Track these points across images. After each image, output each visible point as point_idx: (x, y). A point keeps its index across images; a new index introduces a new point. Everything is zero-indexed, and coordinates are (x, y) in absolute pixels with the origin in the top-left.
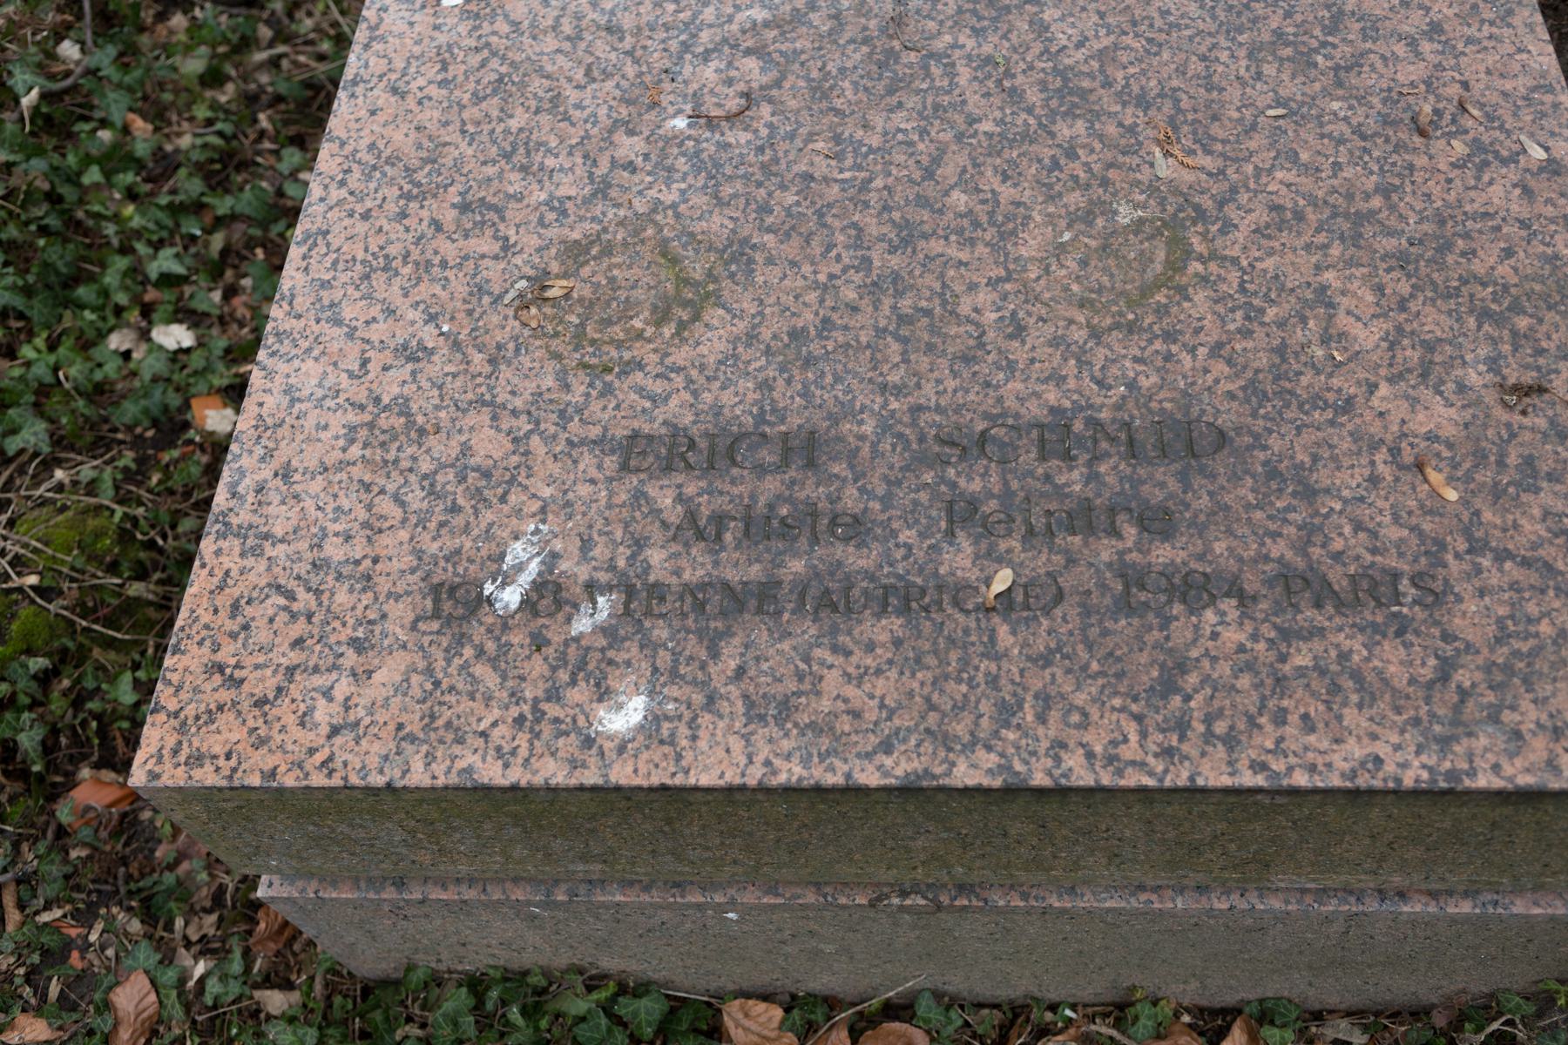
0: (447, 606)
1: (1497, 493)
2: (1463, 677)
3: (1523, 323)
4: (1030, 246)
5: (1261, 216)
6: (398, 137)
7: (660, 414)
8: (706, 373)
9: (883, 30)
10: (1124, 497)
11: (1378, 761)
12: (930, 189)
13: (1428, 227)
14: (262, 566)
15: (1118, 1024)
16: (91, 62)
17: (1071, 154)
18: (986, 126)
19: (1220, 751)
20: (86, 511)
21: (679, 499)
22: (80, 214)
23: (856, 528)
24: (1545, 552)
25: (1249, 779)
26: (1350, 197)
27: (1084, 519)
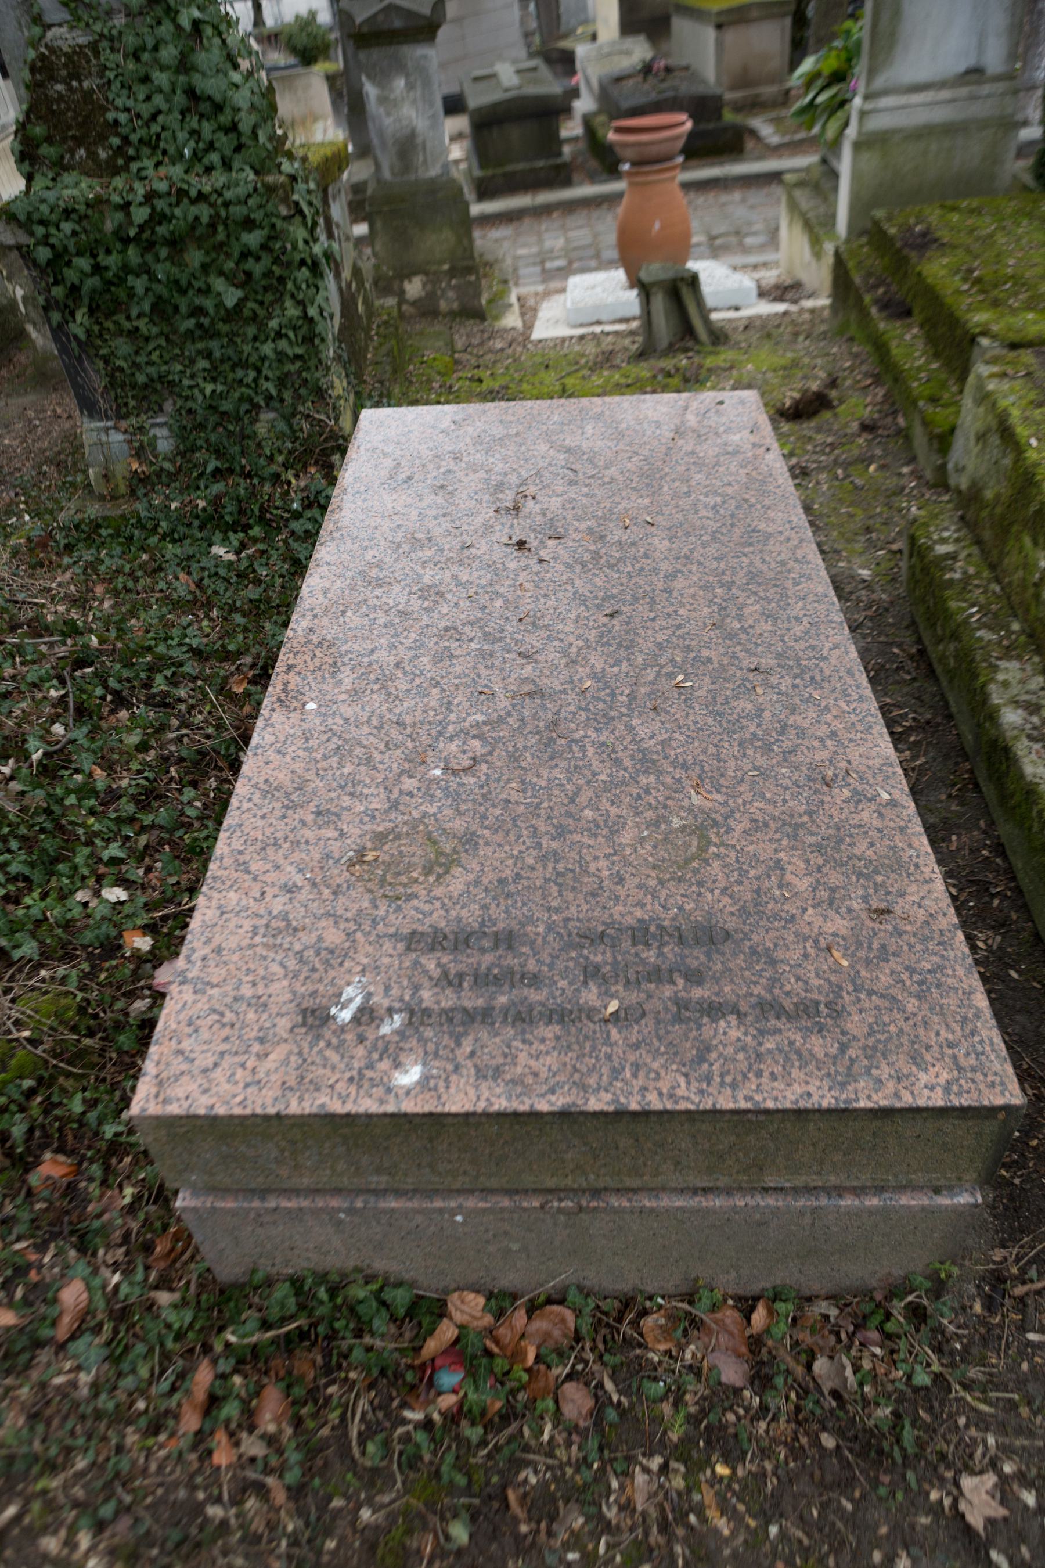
0: (310, 1020)
1: (868, 962)
2: (852, 1053)
3: (879, 879)
4: (626, 837)
5: (746, 824)
6: (281, 776)
7: (428, 921)
8: (452, 899)
9: (547, 728)
10: (679, 964)
11: (809, 1095)
12: (573, 808)
13: (831, 831)
14: (205, 999)
15: (691, 1303)
16: (71, 735)
17: (648, 792)
18: (603, 777)
19: (728, 1091)
20: (60, 994)
21: (439, 965)
22: (64, 822)
23: (535, 980)
24: (893, 991)
25: (743, 1105)
26: (792, 816)
27: (656, 975)
